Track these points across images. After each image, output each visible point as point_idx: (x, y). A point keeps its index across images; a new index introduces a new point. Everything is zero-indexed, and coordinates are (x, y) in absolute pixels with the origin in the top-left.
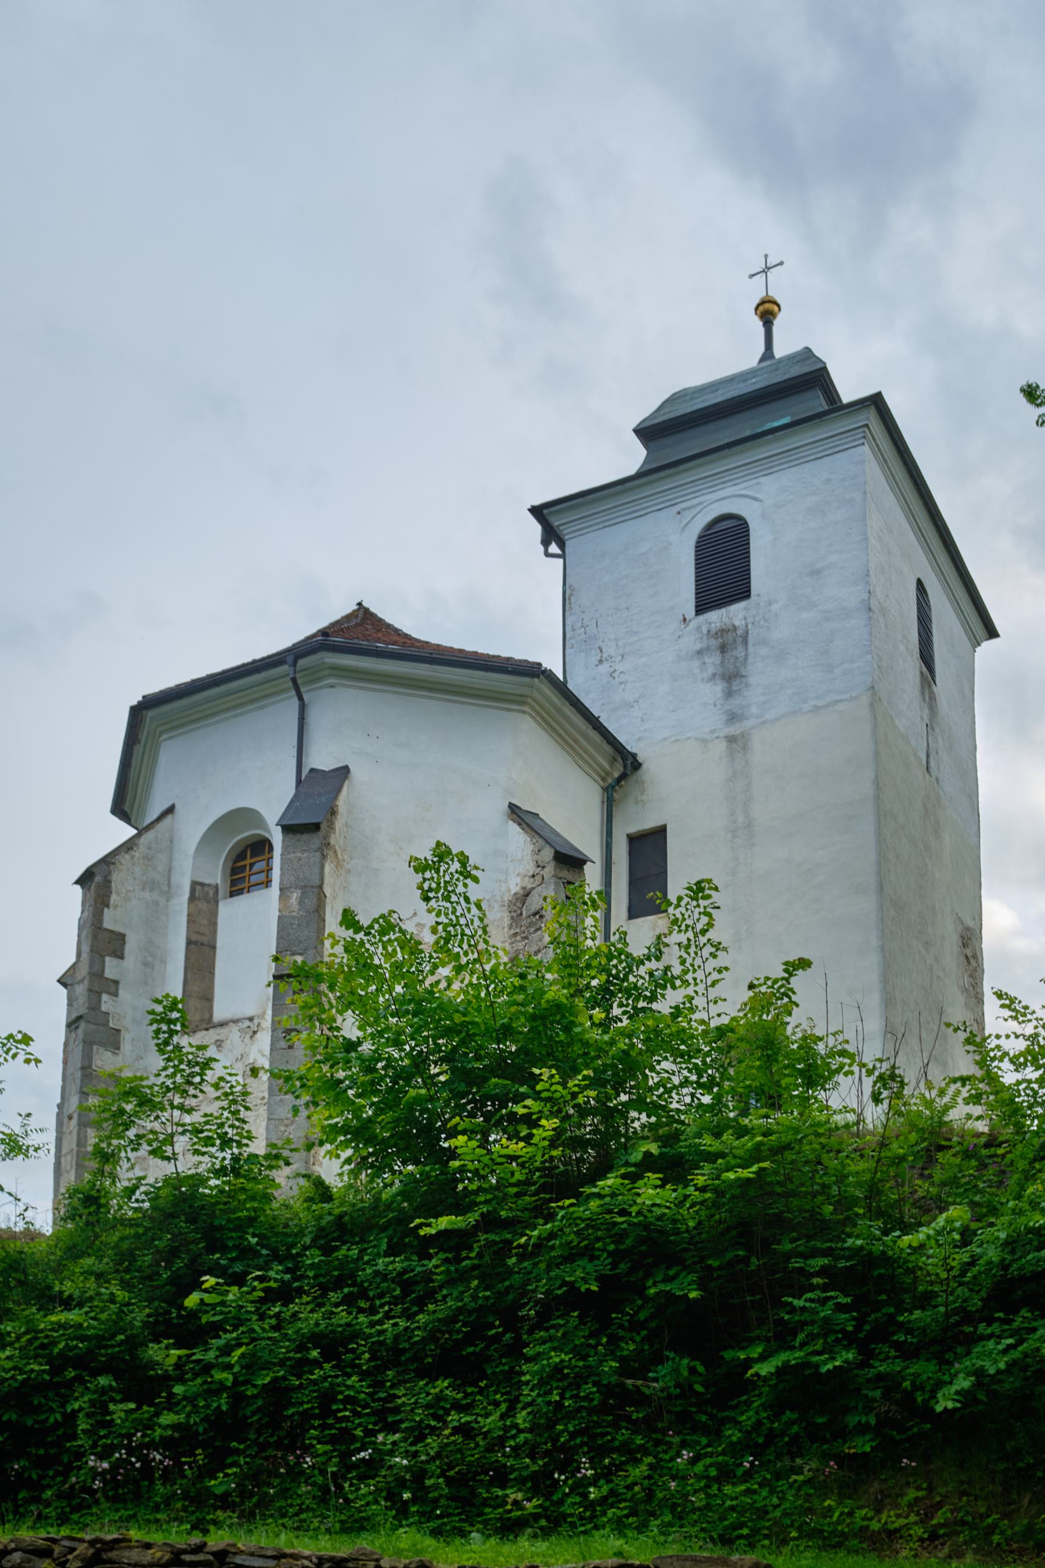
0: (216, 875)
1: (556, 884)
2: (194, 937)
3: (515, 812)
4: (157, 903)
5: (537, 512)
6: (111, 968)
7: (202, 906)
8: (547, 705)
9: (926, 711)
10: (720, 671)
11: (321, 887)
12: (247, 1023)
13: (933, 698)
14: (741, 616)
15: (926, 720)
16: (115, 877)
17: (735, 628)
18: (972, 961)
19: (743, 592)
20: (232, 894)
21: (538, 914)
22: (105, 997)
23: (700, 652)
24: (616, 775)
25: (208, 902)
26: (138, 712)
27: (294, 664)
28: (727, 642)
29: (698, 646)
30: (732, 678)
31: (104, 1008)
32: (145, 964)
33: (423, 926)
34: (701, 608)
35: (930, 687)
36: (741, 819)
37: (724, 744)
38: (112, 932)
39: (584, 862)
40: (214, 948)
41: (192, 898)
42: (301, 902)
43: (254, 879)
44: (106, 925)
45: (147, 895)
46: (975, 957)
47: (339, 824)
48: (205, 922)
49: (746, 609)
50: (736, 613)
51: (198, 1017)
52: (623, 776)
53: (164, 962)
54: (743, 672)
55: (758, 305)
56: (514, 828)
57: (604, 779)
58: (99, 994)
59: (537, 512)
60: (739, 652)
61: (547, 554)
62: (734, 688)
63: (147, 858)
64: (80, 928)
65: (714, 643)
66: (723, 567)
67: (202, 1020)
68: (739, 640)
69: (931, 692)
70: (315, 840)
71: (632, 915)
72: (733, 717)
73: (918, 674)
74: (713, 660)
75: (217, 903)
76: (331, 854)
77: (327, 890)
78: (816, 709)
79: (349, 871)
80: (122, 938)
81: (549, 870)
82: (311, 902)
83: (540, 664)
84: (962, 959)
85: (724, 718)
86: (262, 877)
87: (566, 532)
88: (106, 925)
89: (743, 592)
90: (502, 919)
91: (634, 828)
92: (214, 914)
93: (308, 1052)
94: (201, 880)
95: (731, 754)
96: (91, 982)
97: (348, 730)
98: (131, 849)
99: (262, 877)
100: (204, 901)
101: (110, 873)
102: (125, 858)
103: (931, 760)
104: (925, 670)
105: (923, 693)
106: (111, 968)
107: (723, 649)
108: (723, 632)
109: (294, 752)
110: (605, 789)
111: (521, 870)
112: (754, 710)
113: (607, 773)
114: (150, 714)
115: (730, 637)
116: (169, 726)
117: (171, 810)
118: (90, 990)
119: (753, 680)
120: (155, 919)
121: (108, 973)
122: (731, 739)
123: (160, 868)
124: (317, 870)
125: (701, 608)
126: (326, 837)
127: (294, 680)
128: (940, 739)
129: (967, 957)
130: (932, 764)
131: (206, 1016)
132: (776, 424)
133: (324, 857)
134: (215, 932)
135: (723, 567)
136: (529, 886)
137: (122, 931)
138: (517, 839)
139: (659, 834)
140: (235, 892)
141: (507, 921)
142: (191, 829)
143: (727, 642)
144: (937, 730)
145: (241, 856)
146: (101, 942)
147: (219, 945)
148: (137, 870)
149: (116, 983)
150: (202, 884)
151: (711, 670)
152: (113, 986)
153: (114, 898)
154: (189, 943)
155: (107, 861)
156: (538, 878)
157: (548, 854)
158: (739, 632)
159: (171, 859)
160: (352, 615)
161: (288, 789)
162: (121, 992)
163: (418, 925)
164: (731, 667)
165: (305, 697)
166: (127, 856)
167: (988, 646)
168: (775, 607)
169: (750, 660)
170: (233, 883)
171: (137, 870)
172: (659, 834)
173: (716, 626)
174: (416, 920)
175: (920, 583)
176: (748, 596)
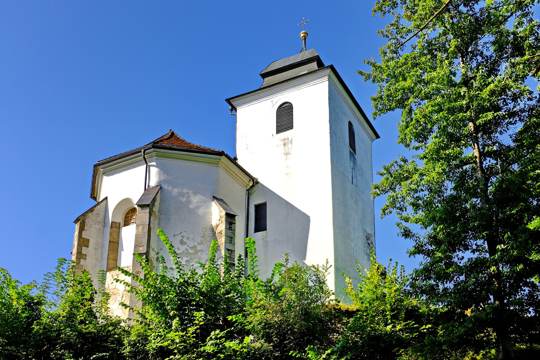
0: (120, 219)
2: (112, 240)
7: (115, 229)
9: (352, 164)
13: (354, 159)
15: (352, 167)
16: (86, 221)
24: (251, 185)
25: (117, 228)
32: (96, 249)
34: (278, 131)
35: (353, 155)
39: (235, 216)
41: (111, 227)
54: (290, 152)
59: (228, 101)
65: (282, 143)
68: (289, 142)
69: (354, 157)
73: (349, 152)
76: (154, 213)
80: (88, 240)
81: (224, 219)
84: (366, 244)
93: (172, 339)
96: (77, 255)
102: (90, 215)
104: (351, 150)
105: (351, 158)
106: (84, 250)
115: (286, 141)
125: (278, 131)
128: (357, 172)
129: (368, 243)
130: (354, 181)
132: (303, 73)
137: (88, 238)
143: (286, 143)
145: (128, 213)
149: (86, 255)
150: (115, 223)
157: (224, 213)
175: (350, 124)
176: (292, 127)
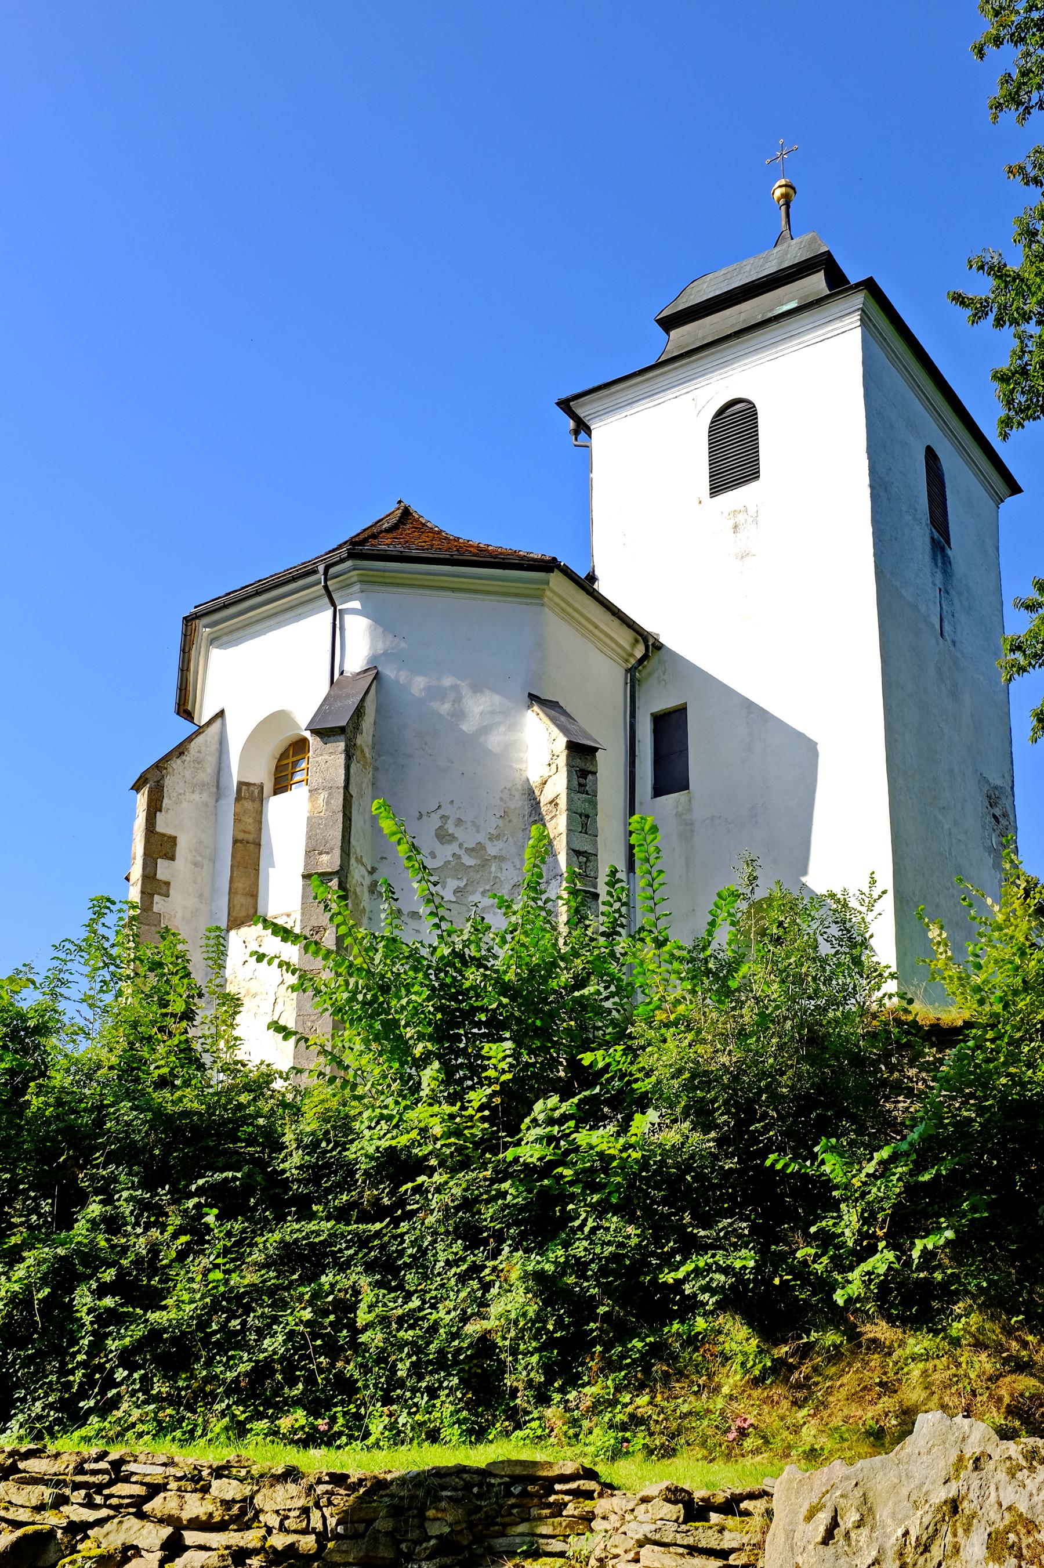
2: (241, 836)
5: (565, 405)
7: (248, 805)
9: (939, 576)
15: (939, 585)
16: (168, 782)
18: (1003, 821)
20: (275, 794)
22: (157, 898)
25: (253, 801)
32: (195, 864)
33: (448, 817)
34: (716, 489)
35: (943, 550)
38: (164, 835)
41: (239, 798)
46: (1005, 815)
48: (251, 821)
59: (565, 405)
71: (658, 792)
73: (928, 540)
76: (358, 753)
80: (173, 840)
102: (176, 764)
103: (946, 624)
104: (936, 535)
105: (934, 558)
116: (570, 610)
117: (221, 714)
121: (161, 875)
125: (716, 489)
127: (326, 587)
128: (956, 601)
129: (995, 816)
130: (947, 627)
136: (546, 775)
139: (681, 711)
140: (276, 792)
144: (952, 592)
145: (284, 756)
148: (188, 774)
149: (168, 884)
150: (248, 784)
152: (164, 887)
154: (235, 842)
155: (160, 766)
156: (554, 767)
162: (171, 892)
163: (443, 817)
166: (179, 761)
167: (1012, 502)
172: (681, 711)
174: (440, 812)
175: (931, 455)
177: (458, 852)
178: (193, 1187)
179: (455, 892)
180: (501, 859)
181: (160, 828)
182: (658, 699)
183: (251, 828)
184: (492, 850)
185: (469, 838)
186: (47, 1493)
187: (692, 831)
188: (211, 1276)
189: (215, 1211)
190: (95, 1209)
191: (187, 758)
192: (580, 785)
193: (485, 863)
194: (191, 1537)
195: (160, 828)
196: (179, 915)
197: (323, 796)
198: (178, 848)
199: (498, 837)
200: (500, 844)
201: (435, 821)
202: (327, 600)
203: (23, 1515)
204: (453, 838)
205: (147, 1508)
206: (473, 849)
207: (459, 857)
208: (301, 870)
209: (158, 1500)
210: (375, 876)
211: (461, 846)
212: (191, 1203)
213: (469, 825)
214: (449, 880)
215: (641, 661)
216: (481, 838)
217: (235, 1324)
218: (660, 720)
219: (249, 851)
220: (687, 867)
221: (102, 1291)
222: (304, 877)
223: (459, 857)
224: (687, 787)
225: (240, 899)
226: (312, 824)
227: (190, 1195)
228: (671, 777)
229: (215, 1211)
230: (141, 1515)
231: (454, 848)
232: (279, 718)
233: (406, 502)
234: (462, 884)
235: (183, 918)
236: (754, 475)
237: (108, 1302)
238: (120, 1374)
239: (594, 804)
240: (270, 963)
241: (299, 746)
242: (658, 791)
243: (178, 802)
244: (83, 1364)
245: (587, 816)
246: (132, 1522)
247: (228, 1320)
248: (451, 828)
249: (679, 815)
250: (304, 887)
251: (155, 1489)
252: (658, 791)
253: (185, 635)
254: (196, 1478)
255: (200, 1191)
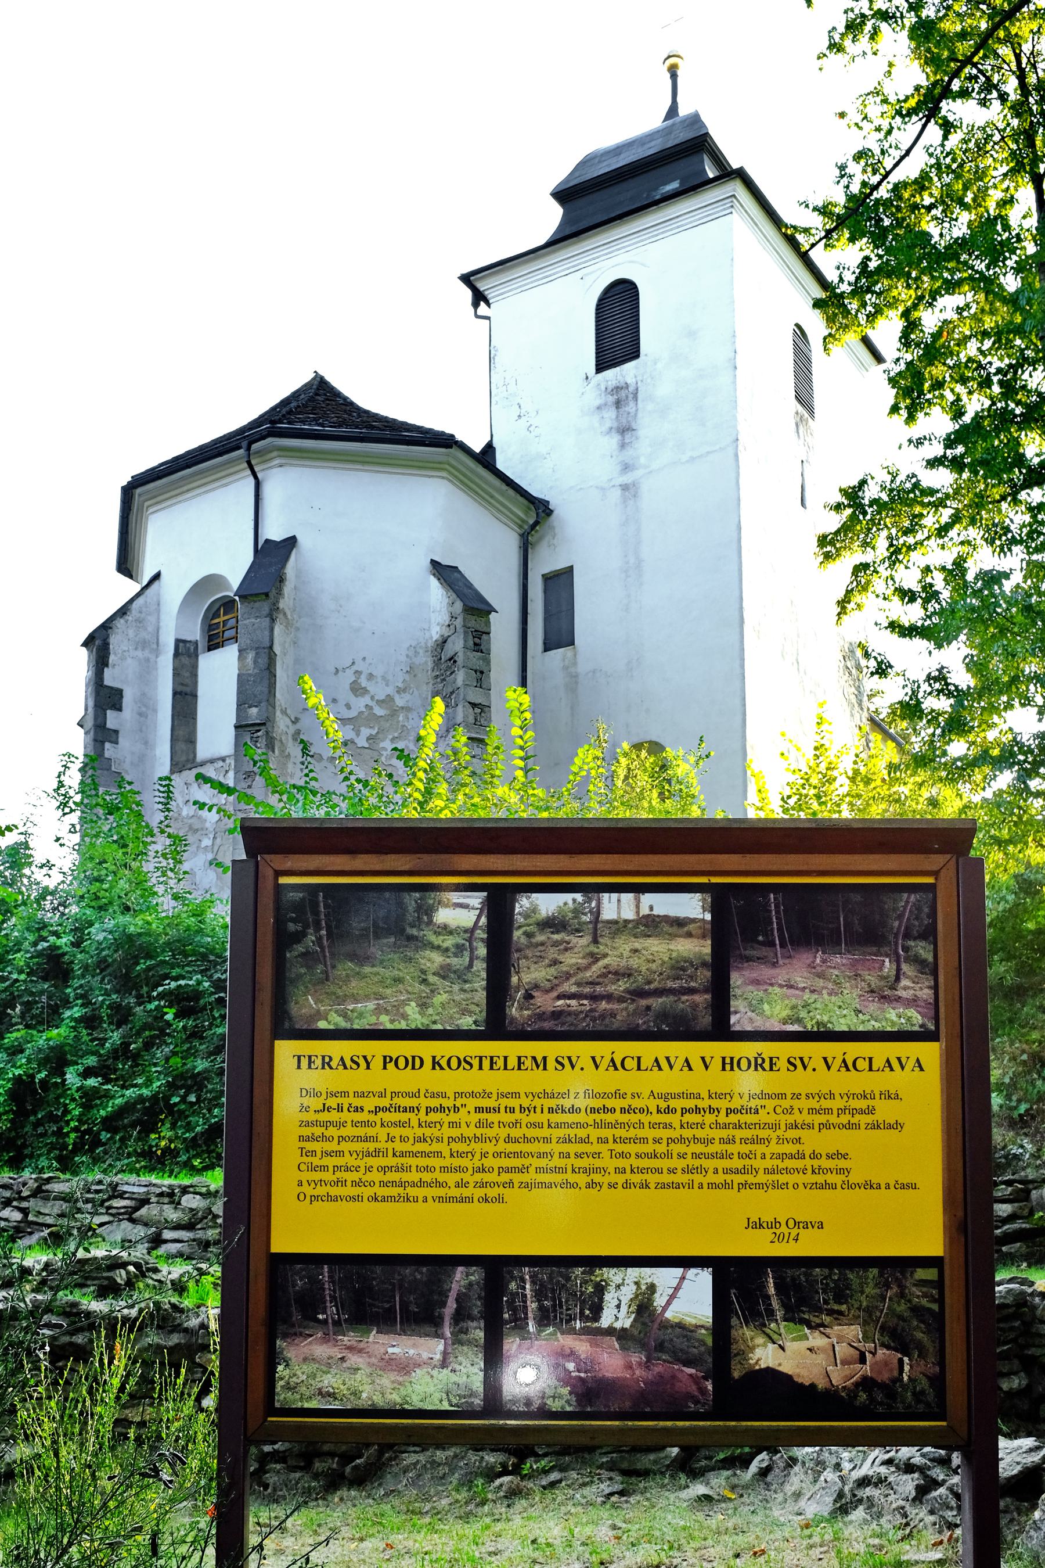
0: (195, 633)
1: (465, 633)
2: (179, 689)
3: (438, 568)
4: (148, 660)
5: (467, 279)
6: (112, 719)
7: (185, 660)
8: (464, 470)
10: (615, 425)
11: (271, 647)
12: (221, 763)
14: (632, 375)
17: (627, 386)
19: (634, 353)
20: (209, 650)
21: (452, 659)
22: (107, 745)
23: (599, 408)
24: (531, 522)
25: (189, 656)
26: (128, 492)
27: (249, 449)
28: (621, 398)
29: (598, 402)
30: (625, 430)
31: (107, 755)
32: (140, 714)
34: (600, 368)
36: (632, 560)
37: (618, 492)
40: (196, 696)
41: (177, 654)
42: (255, 662)
43: (227, 634)
44: (106, 683)
45: (139, 653)
47: (288, 589)
49: (636, 368)
50: (628, 372)
51: (184, 758)
52: (537, 523)
53: (155, 711)
55: (669, 57)
56: (434, 582)
57: (520, 527)
58: (103, 743)
59: (467, 279)
60: (631, 407)
61: (477, 316)
62: (627, 441)
63: (139, 621)
64: (87, 685)
65: (611, 399)
66: (619, 324)
67: (188, 761)
68: (631, 396)
70: (265, 607)
71: (547, 647)
72: (626, 468)
74: (611, 414)
75: (197, 656)
76: (281, 616)
77: (277, 649)
78: (692, 459)
79: (298, 629)
80: (119, 693)
82: (263, 661)
83: (453, 436)
85: (619, 468)
86: (232, 633)
87: (490, 295)
88: (106, 683)
89: (635, 354)
90: (426, 663)
91: (546, 571)
92: (195, 667)
94: (183, 638)
95: (625, 501)
96: (95, 732)
97: (300, 496)
98: (125, 613)
99: (232, 633)
100: (186, 655)
101: (108, 637)
102: (120, 623)
106: (112, 719)
107: (618, 404)
108: (618, 389)
109: (252, 524)
110: (522, 535)
111: (439, 619)
112: (642, 460)
113: (523, 521)
114: (138, 491)
117: (157, 577)
118: (95, 740)
119: (641, 433)
120: (148, 669)
121: (111, 724)
122: (625, 488)
123: (150, 629)
124: (267, 633)
125: (600, 368)
126: (275, 604)
131: (191, 756)
133: (273, 620)
134: (196, 683)
135: (619, 324)
138: (436, 593)
141: (430, 665)
142: (173, 592)
143: (621, 398)
146: (105, 698)
147: (200, 693)
149: (116, 732)
150: (184, 641)
151: (608, 424)
152: (114, 735)
153: (112, 658)
155: (106, 627)
158: (631, 389)
159: (159, 618)
160: (314, 379)
161: (246, 557)
162: (120, 740)
163: (356, 672)
164: (624, 421)
165: (259, 475)
166: (122, 621)
168: (659, 366)
169: (640, 415)
170: (211, 638)
171: (131, 633)
173: (612, 384)
174: (355, 668)
177: (370, 703)
178: (155, 994)
179: (368, 739)
180: (407, 709)
181: (108, 682)
182: (545, 562)
183: (188, 681)
184: (400, 701)
185: (380, 691)
186: (65, 1206)
187: (577, 683)
188: (172, 1061)
189: (174, 1010)
190: (77, 1012)
191: (129, 618)
192: (475, 644)
193: (394, 713)
194: (167, 1235)
195: (108, 682)
196: (128, 760)
197: (250, 656)
198: (125, 700)
199: (404, 690)
200: (407, 696)
201: (349, 677)
202: (249, 472)
203: (49, 1220)
204: (365, 691)
205: (135, 1216)
206: (383, 701)
207: (371, 708)
208: (232, 720)
209: (143, 1211)
210: (298, 726)
211: (372, 698)
212: (152, 1006)
213: (379, 679)
214: (362, 729)
215: (533, 527)
216: (390, 690)
217: (192, 1098)
218: (549, 579)
219: (185, 699)
220: (572, 715)
221: (87, 1073)
222: (236, 727)
223: (371, 708)
224: (572, 643)
225: (181, 746)
226: (242, 680)
227: (151, 999)
228: (561, 635)
229: (174, 1010)
230: (132, 1221)
231: (366, 700)
232: (210, 582)
233: (321, 373)
234: (374, 732)
235: (132, 763)
236: (634, 353)
237: (92, 1082)
238: (104, 1136)
239: (488, 662)
240: (210, 810)
241: (228, 604)
242: (548, 646)
243: (123, 659)
244: (76, 1129)
245: (482, 672)
246: (125, 1224)
247: (186, 1095)
248: (363, 682)
249: (565, 668)
250: (237, 737)
251: (144, 1202)
252: (548, 646)
253: (127, 532)
254: (171, 1195)
255: (161, 996)
